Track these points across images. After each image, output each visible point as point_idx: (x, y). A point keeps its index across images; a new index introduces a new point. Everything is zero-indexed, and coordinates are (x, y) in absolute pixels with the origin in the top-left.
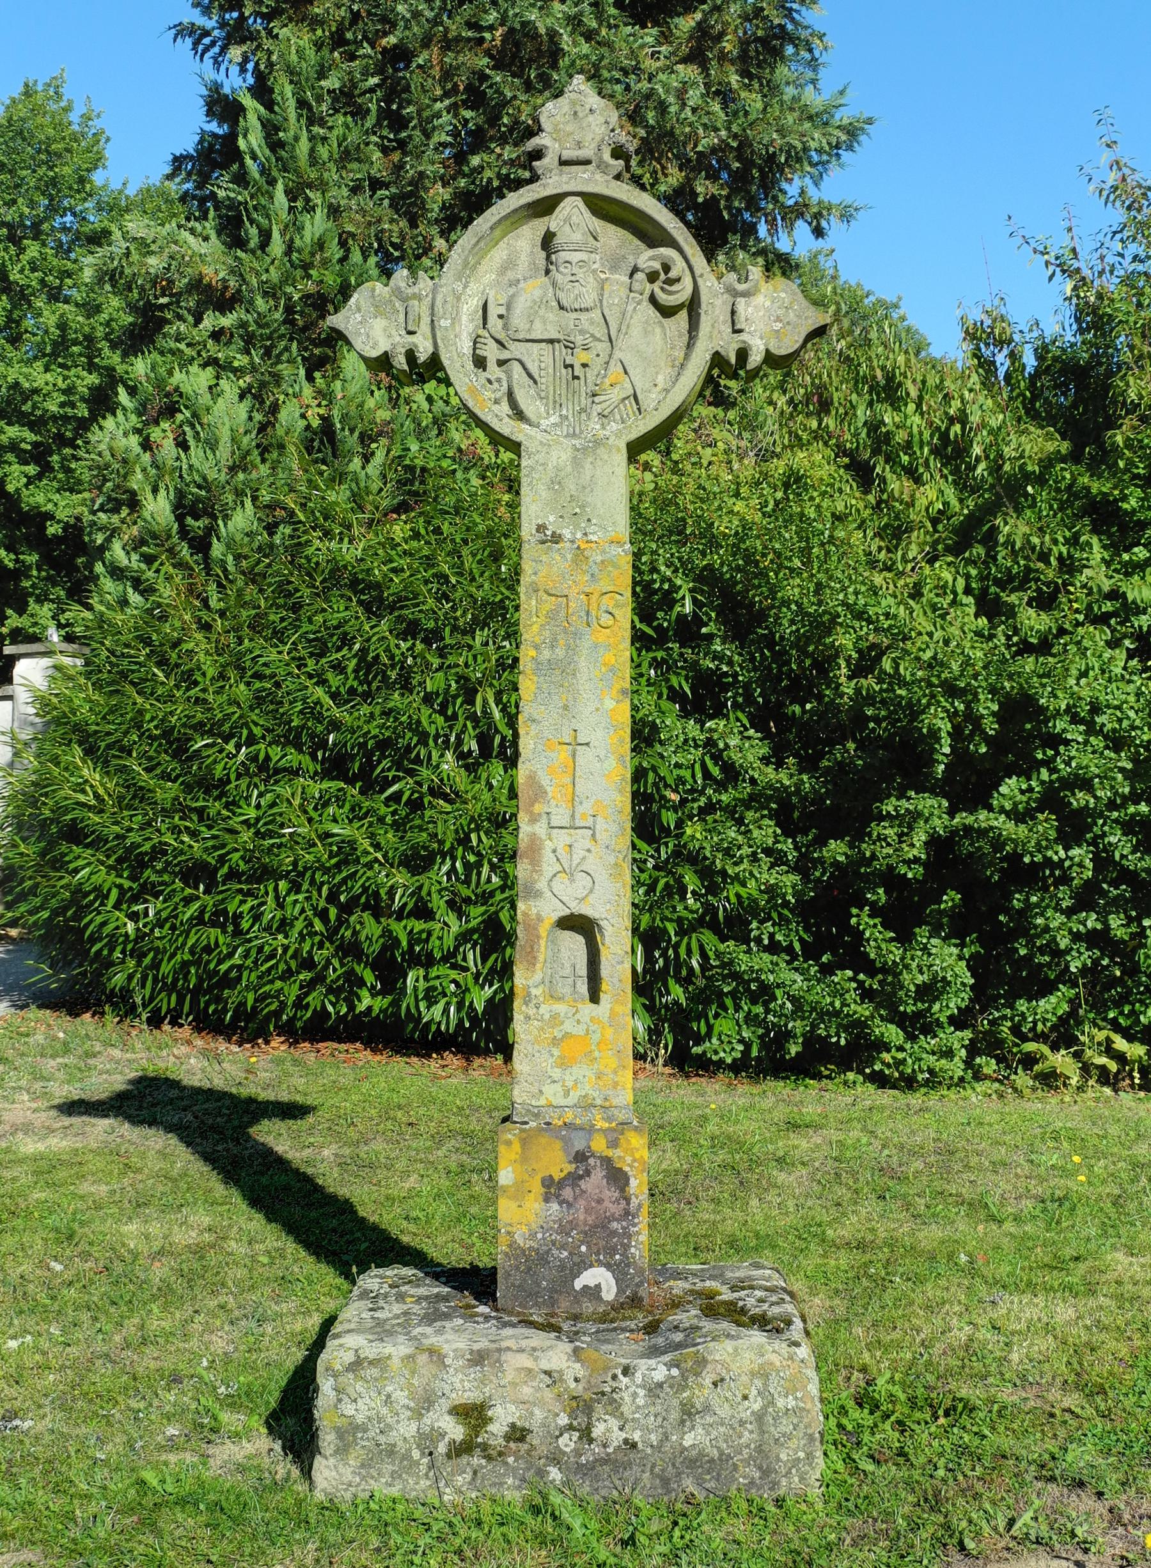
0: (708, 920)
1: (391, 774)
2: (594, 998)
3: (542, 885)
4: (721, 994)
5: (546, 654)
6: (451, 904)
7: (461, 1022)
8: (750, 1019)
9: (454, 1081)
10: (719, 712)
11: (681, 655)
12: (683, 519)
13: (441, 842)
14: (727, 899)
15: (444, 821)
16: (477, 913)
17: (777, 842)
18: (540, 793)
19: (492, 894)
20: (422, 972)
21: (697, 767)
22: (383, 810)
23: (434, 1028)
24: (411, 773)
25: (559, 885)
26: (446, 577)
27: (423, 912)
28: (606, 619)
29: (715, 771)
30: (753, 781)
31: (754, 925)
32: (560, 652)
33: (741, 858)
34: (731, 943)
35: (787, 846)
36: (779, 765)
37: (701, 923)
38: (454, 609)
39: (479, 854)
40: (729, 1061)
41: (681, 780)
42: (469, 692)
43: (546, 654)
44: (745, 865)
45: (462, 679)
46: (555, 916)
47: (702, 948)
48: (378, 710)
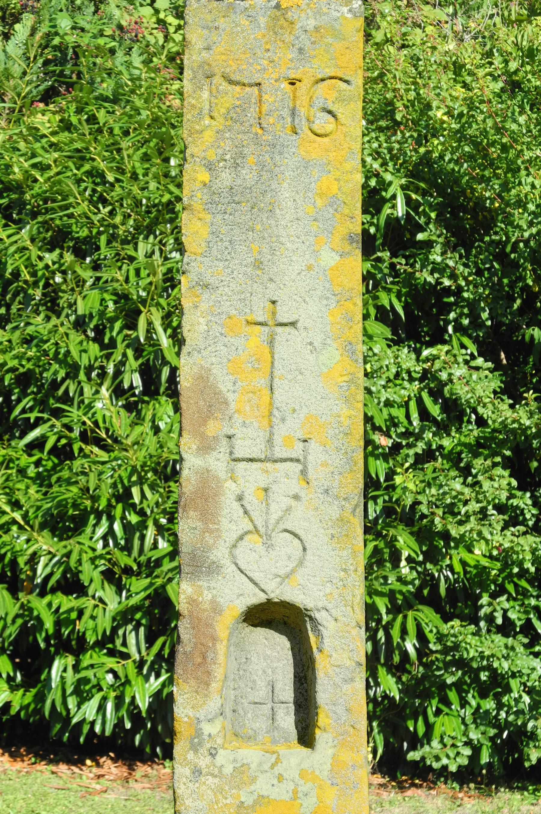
0: (427, 594)
1: (33, 416)
2: (306, 736)
3: (220, 553)
4: (443, 687)
5: (226, 178)
6: (108, 575)
7: (120, 723)
8: (480, 717)
9: (111, 797)
10: (438, 338)
11: (392, 266)
12: (390, 103)
13: (95, 499)
14: (451, 568)
15: (97, 474)
16: (139, 588)
17: (511, 496)
18: (216, 404)
19: (158, 563)
20: (70, 660)
21: (413, 405)
22: (25, 460)
23: (86, 729)
24: (57, 413)
25: (249, 554)
26: (102, 176)
27: (72, 585)
28: (324, 122)
29: (435, 410)
30: (481, 422)
31: (485, 599)
32: (248, 175)
33: (467, 516)
34: (456, 623)
35: (524, 501)
36: (517, 399)
37: (417, 598)
38: (112, 213)
39: (142, 513)
40: (453, 768)
41: (393, 422)
42: (131, 315)
43: (226, 178)
44: (473, 523)
45: (122, 297)
46: (241, 605)
47: (419, 627)
48: (16, 336)
